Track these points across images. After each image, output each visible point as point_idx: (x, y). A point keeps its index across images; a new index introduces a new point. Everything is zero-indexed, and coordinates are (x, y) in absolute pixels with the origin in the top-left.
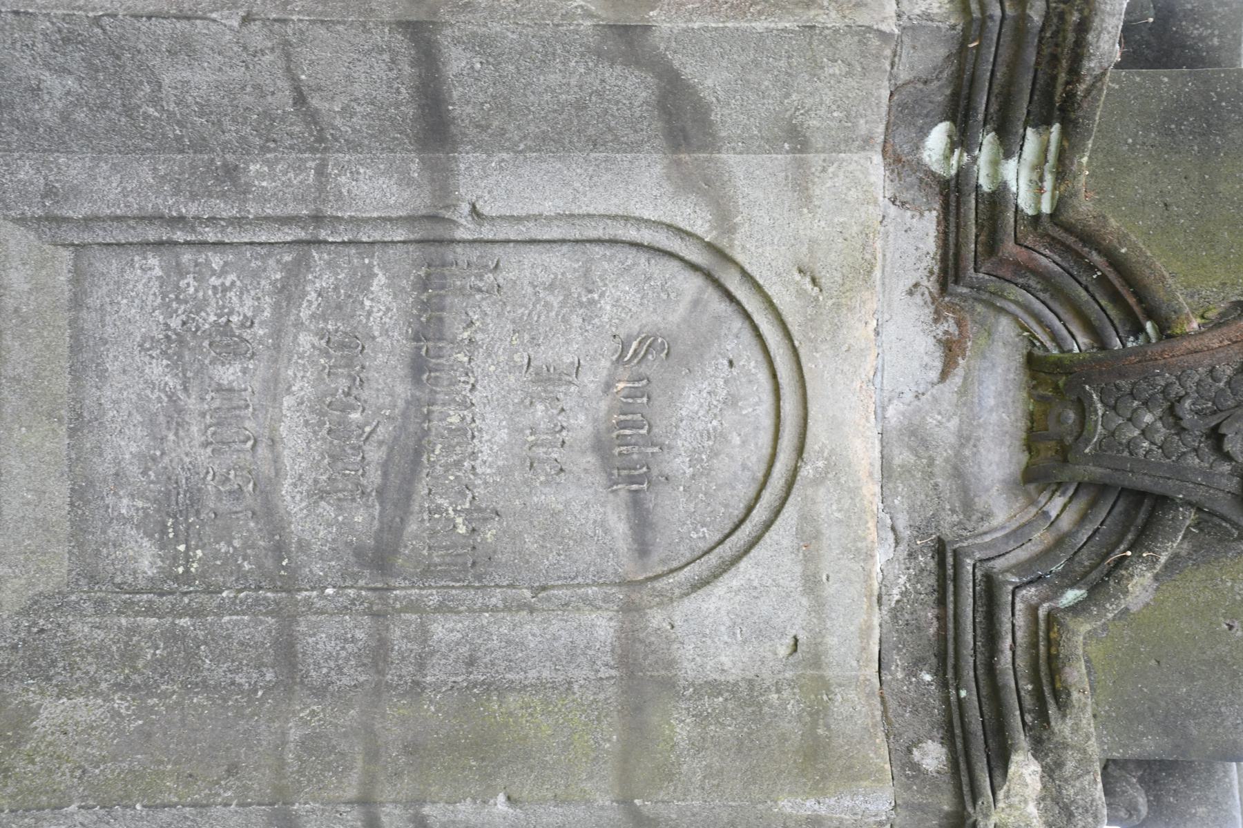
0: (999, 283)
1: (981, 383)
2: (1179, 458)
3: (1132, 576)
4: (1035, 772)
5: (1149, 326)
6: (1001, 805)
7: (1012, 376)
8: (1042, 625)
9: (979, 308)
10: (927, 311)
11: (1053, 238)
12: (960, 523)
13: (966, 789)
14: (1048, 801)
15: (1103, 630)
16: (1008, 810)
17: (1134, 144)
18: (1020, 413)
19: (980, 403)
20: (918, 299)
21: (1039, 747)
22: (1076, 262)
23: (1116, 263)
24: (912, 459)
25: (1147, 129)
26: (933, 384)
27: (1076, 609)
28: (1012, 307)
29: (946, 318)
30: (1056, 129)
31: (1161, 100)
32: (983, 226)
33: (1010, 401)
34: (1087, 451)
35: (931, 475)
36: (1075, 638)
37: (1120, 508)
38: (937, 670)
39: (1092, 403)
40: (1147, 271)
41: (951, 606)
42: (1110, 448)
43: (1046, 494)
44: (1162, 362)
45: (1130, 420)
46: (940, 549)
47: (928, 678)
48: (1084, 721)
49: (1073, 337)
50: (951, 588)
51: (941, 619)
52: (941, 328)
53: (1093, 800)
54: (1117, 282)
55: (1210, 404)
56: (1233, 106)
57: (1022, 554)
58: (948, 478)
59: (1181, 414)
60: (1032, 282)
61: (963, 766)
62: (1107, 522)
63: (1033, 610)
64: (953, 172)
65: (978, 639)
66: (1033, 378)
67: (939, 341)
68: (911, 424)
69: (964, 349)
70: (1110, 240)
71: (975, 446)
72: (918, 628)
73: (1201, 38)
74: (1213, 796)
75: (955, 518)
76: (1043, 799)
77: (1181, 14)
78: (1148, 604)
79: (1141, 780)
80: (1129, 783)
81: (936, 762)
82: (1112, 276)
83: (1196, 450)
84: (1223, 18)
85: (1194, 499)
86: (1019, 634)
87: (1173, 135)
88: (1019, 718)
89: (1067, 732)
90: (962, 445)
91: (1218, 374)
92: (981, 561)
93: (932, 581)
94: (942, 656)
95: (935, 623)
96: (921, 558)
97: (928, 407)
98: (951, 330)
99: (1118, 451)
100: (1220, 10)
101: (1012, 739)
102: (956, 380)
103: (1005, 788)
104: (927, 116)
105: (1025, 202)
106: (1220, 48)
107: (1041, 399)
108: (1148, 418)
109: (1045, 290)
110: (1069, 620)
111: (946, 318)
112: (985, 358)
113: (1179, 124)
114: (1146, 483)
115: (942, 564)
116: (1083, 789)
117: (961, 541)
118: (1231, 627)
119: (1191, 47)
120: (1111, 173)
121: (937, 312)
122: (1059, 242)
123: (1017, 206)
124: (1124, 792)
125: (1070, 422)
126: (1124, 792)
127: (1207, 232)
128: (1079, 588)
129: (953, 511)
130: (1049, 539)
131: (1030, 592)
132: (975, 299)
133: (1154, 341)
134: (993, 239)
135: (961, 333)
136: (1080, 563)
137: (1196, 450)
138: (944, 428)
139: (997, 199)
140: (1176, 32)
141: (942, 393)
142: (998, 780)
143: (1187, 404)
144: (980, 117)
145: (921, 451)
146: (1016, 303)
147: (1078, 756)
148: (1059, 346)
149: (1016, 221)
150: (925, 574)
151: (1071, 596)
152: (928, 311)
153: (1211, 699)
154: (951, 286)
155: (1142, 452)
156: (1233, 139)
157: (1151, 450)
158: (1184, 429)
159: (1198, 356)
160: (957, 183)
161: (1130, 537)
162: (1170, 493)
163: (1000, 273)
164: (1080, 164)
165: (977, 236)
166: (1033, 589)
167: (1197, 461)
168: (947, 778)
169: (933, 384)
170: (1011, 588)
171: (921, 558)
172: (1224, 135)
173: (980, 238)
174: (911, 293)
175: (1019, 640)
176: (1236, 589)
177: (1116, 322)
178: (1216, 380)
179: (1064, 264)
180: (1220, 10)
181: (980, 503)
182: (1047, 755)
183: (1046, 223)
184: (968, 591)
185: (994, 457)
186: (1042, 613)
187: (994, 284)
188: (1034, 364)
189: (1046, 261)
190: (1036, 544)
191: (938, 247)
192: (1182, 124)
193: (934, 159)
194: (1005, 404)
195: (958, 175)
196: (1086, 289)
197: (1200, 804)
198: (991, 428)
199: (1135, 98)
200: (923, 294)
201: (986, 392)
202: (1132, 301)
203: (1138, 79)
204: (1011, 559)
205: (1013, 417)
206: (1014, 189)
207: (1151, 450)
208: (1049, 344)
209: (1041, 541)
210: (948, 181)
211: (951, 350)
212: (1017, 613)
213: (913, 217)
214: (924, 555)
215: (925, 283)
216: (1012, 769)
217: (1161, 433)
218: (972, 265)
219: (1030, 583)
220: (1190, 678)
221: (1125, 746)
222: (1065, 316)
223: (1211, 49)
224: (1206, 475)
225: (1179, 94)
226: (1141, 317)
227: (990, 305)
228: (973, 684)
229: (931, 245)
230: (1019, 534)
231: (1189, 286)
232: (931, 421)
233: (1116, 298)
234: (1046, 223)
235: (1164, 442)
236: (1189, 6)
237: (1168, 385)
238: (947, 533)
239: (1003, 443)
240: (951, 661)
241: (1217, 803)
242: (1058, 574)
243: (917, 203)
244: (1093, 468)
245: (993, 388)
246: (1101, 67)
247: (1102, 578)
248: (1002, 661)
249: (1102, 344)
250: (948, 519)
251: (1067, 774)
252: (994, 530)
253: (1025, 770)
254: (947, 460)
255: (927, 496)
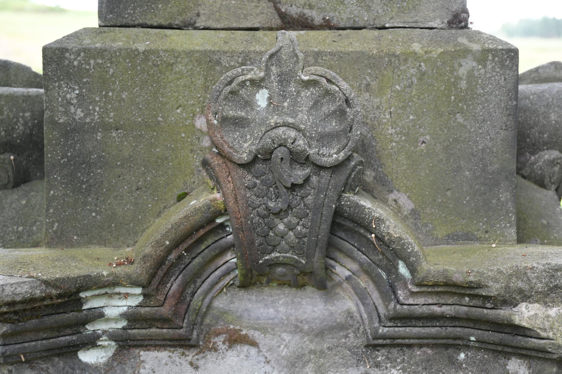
0: (190, 312)
1: (258, 318)
2: (308, 208)
3: (388, 233)
4: (527, 308)
5: (219, 221)
6: (551, 335)
7: (254, 297)
8: (424, 289)
9: (207, 321)
10: (209, 356)
11: (159, 283)
12: (354, 332)
13: (540, 355)
14: (547, 300)
15: (427, 226)
16: (555, 331)
17: (96, 211)
18: (279, 292)
19: (273, 319)
20: (201, 363)
21: (508, 301)
22: (176, 267)
23: (176, 245)
24: (311, 365)
25: (85, 204)
26: (260, 351)
27: (412, 269)
28: (207, 300)
29: (215, 343)
30: (83, 295)
31: (65, 195)
32: (151, 324)
33: (270, 299)
34: (304, 262)
35: (322, 352)
36: (432, 272)
37: (343, 235)
38: (457, 348)
39: (271, 260)
40: (182, 227)
41: (412, 341)
42: (302, 249)
43: (334, 277)
44: (243, 220)
45: (282, 237)
46: (373, 347)
47: (462, 356)
48: (490, 274)
49: (227, 262)
50: (399, 341)
51: (421, 346)
52: (221, 346)
53: (545, 271)
54: (190, 242)
55: (271, 189)
56: (70, 148)
57: (375, 296)
58: (324, 340)
59: (278, 210)
60: (189, 291)
61: (524, 352)
62: (352, 243)
63: (413, 294)
64: (113, 343)
65: (434, 324)
66: (255, 284)
67: (230, 347)
68: (287, 366)
69: (235, 330)
70: (160, 251)
71: (301, 322)
72: (428, 361)
73: (25, 124)
74: (543, 109)
75: (351, 335)
76: (545, 303)
77: (8, 137)
78: (409, 197)
79: (533, 153)
80: (534, 163)
81: (522, 367)
82: (185, 245)
83: (302, 198)
84: (11, 111)
85: (336, 197)
86: (430, 301)
87: (90, 186)
88: (489, 311)
89: (498, 286)
90: (301, 331)
91: (251, 184)
92: (380, 321)
93: (395, 351)
94: (447, 346)
95: (424, 349)
96: (379, 359)
97: (275, 355)
98: (222, 339)
99: (304, 244)
100: (6, 113)
101: (503, 320)
102: (256, 335)
103: (539, 331)
104: (73, 369)
105: (134, 302)
106: (32, 111)
107: (268, 282)
108: (281, 227)
109: (195, 282)
110: (420, 275)
111: (214, 343)
112: (241, 316)
113: (83, 182)
114: (325, 227)
115: (383, 346)
116: (537, 278)
117: (367, 333)
118: (424, 142)
119: (31, 130)
120: (116, 226)
121: (210, 350)
122: (162, 280)
123: (137, 306)
124: (541, 169)
125: (284, 270)
126: (541, 169)
127: (156, 162)
128: (398, 264)
129: (346, 336)
130: (364, 277)
131: (401, 294)
132: (201, 324)
133: (228, 217)
134: (160, 320)
135: (224, 333)
136: (380, 261)
137: (302, 198)
138: (289, 343)
139: (133, 318)
140: (21, 140)
141: (265, 345)
142: (532, 334)
143: (271, 205)
144: (74, 338)
145: (306, 359)
146: (203, 300)
147: (514, 279)
148: (233, 270)
149: (147, 306)
150: (390, 356)
151: (403, 269)
152: (211, 356)
153: (473, 155)
154: (192, 342)
155: (304, 230)
156: (93, 147)
157: (303, 225)
158: (289, 206)
159: (238, 197)
160: (122, 341)
161: (362, 231)
162: (332, 212)
163: (183, 312)
164: (108, 275)
165: (158, 328)
166: (399, 292)
167: (310, 197)
168: (534, 364)
169: (260, 351)
170: (398, 306)
171: (379, 359)
172: (91, 153)
173: (159, 326)
174: (197, 368)
175: (435, 301)
176: (397, 139)
177: (216, 239)
178: (255, 185)
179: (177, 274)
180: (6, 113)
181: (340, 319)
182: (514, 298)
183: (149, 290)
184: (401, 331)
185: (309, 309)
186: (415, 289)
187: (191, 316)
188: (246, 284)
189: (174, 285)
190: (368, 285)
191: (165, 350)
192: (83, 181)
193: (104, 355)
194: (273, 302)
195: (115, 341)
196: (193, 258)
197: (549, 117)
198: (289, 311)
199: (65, 212)
200: (198, 359)
201: (264, 315)
202: (202, 232)
203: (51, 211)
204: (379, 302)
205: (282, 296)
206: (125, 309)
207: (303, 225)
208: (232, 276)
209: (366, 282)
210: (120, 346)
211: (236, 339)
212: (416, 303)
213: (145, 368)
214: (377, 357)
215: (189, 358)
216: (524, 324)
217: (291, 219)
218: (177, 331)
219: (395, 293)
220: (459, 169)
221: (507, 212)
222: (210, 271)
223: (33, 118)
224: (319, 192)
225: (63, 183)
226: (213, 226)
227: (205, 314)
228: (466, 330)
229: (163, 355)
230: (362, 296)
231: (193, 173)
232: (285, 352)
233: (200, 241)
234: (149, 290)
235: (297, 217)
236: (3, 133)
237: (259, 215)
238: (360, 341)
239: (299, 303)
240: (451, 342)
241: (547, 106)
242: (388, 275)
243: (134, 365)
244: (316, 258)
245: (262, 310)
246: (40, 286)
247: (390, 252)
248: (450, 312)
249: (229, 247)
250: (352, 340)
251: (527, 287)
252: (359, 311)
253: (525, 314)
254: (311, 341)
255: (336, 355)
